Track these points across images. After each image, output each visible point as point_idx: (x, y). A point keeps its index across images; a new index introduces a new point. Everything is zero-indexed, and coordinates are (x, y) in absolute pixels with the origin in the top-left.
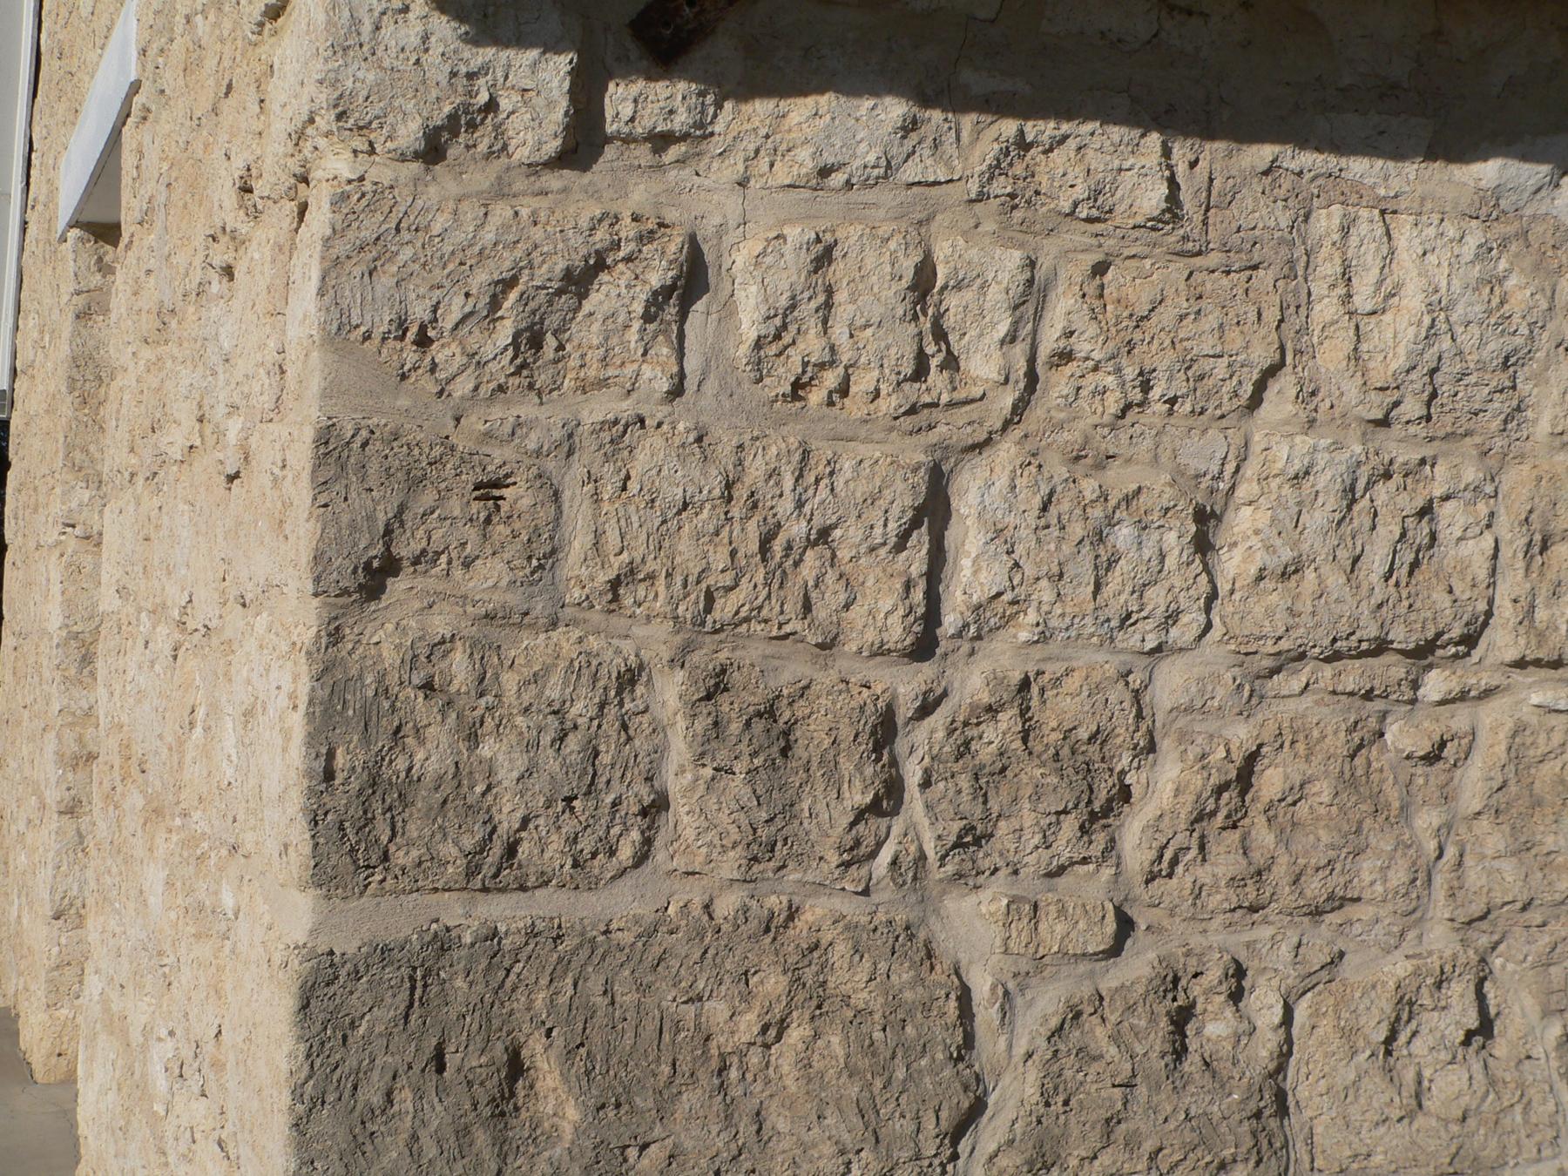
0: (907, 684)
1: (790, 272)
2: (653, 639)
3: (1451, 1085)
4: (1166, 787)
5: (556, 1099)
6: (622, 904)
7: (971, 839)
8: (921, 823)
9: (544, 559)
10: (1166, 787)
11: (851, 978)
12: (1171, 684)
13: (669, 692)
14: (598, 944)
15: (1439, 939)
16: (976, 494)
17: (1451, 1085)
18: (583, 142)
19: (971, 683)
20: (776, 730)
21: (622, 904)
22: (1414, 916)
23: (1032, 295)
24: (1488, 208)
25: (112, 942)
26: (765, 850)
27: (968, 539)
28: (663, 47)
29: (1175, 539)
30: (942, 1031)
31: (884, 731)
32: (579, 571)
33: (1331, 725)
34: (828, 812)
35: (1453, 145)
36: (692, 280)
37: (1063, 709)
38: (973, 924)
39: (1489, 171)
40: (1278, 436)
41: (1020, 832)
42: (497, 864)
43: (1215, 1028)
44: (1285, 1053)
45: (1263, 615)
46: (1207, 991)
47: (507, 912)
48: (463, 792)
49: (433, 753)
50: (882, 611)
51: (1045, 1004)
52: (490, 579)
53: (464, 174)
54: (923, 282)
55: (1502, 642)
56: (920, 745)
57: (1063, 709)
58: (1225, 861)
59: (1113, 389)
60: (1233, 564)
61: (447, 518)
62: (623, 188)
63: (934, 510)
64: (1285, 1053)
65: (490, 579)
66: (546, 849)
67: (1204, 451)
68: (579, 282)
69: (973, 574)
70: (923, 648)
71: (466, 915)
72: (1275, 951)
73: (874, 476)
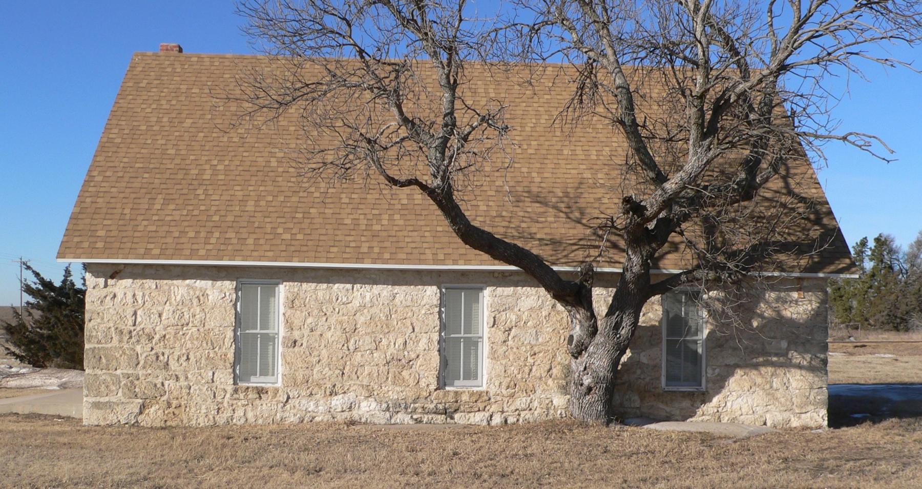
0: (132, 328)
1: (122, 295)
2: (112, 325)
3: (184, 364)
4: (157, 337)
5: (104, 360)
6: (109, 345)
7: (138, 341)
8: (133, 340)
9: (103, 319)
10: (157, 337)
11: (127, 352)
12: (157, 329)
13: (113, 329)
14: (107, 349)
15: (184, 351)
16: (139, 313)
17: (184, 364)
18: (106, 286)
19: (138, 329)
20: (121, 332)
21: (109, 345)
22: (181, 349)
23: (144, 296)
24: (188, 285)
25: (418, 52)
26: (120, 341)
27: (138, 316)
28: (112, 277)
29: (157, 316)
30: (135, 357)
31: (130, 332)
32: (106, 320)
33: (173, 332)
34: (125, 338)
35: (185, 278)
36: (115, 296)
37: (147, 331)
38: (138, 348)
39: (188, 282)
40: (167, 307)
41: (142, 340)
42: (99, 342)
43: (161, 358)
44: (37, 275)
45: (165, 322)
46: (160, 355)
47: (100, 346)
48: (96, 337)
49: (94, 334)
50: (130, 323)
51: (144, 355)
52: (99, 320)
53: (97, 289)
54: (134, 295)
55: (190, 324)
56: (134, 333)
57: (147, 331)
58: (162, 343)
59: (151, 303)
60: (163, 318)
61: (95, 316)
62: (109, 289)
63: (135, 314)
64: (37, 275)
65: (99, 320)
66: (103, 341)
67: (160, 309)
68: (105, 297)
69: (139, 319)
70: (134, 325)
71: (97, 346)
72: (167, 352)
73: (130, 311)
